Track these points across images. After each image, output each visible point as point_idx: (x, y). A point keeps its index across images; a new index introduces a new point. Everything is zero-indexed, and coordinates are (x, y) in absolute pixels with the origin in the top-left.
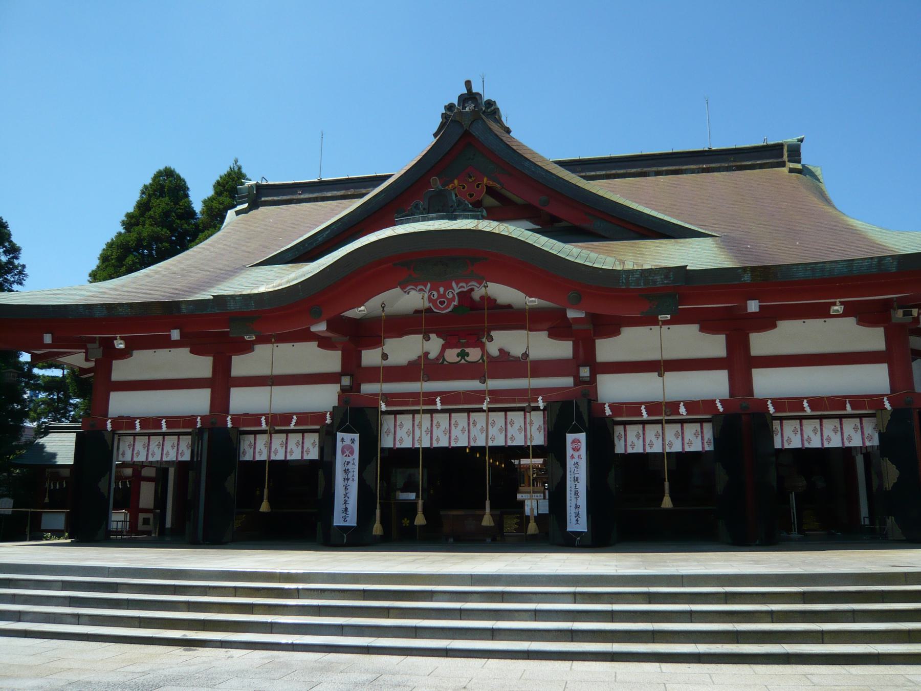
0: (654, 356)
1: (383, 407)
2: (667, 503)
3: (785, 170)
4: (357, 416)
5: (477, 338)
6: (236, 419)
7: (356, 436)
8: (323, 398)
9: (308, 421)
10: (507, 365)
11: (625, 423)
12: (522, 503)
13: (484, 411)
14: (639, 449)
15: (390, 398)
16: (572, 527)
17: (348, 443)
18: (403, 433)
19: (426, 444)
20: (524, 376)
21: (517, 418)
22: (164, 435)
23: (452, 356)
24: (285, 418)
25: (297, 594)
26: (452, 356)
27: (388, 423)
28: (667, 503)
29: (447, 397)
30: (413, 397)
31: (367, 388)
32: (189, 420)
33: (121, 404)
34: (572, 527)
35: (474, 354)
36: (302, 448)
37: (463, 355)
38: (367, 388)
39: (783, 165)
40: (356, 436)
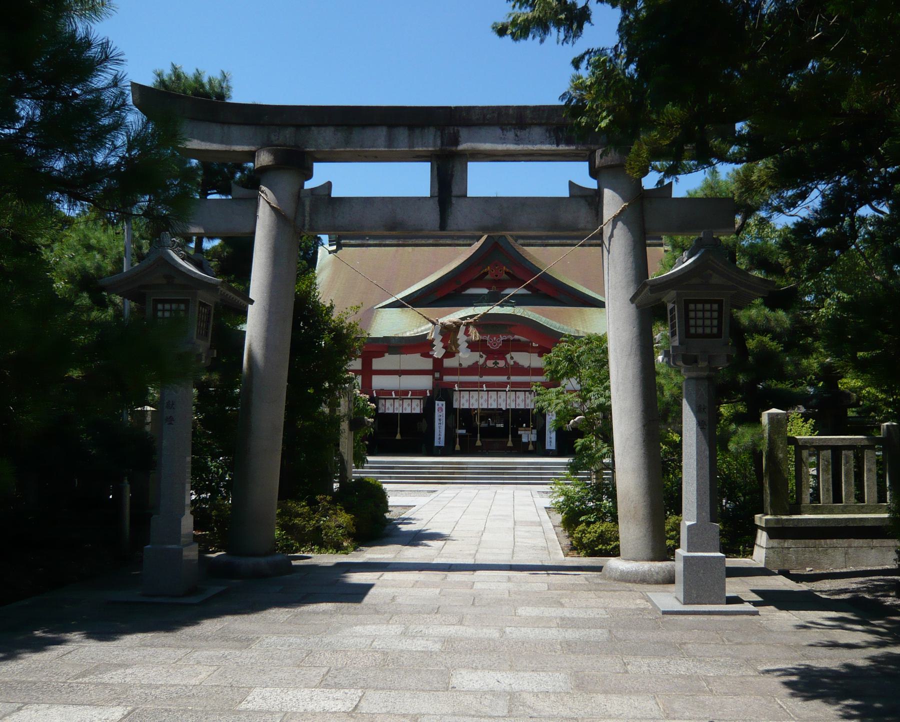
0: (397, 368)
1: (457, 388)
2: (398, 437)
3: (662, 249)
4: (443, 392)
5: (500, 354)
6: (377, 391)
7: (444, 403)
8: (425, 383)
9: (417, 393)
10: (519, 370)
11: (385, 399)
12: (521, 436)
13: (567, 391)
14: (391, 411)
15: (462, 384)
16: (548, 447)
17: (440, 405)
18: (465, 401)
19: (513, 407)
20: (528, 375)
21: (521, 395)
22: (394, 399)
23: (490, 363)
24: (405, 393)
25: (467, 468)
26: (490, 363)
27: (456, 396)
28: (398, 437)
29: (489, 385)
30: (474, 384)
31: (447, 378)
32: (423, 392)
33: (379, 382)
34: (548, 447)
35: (502, 364)
36: (416, 407)
37: (496, 363)
38: (447, 378)
39: (661, 245)
40: (444, 403)
